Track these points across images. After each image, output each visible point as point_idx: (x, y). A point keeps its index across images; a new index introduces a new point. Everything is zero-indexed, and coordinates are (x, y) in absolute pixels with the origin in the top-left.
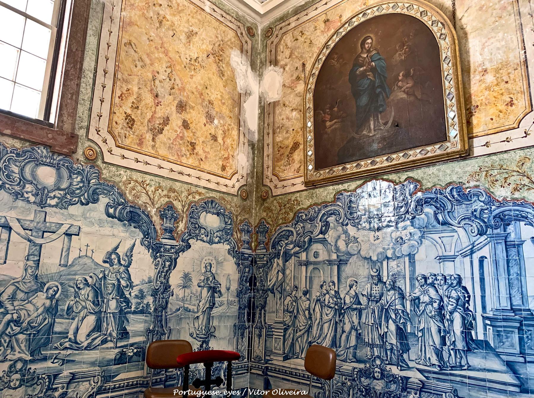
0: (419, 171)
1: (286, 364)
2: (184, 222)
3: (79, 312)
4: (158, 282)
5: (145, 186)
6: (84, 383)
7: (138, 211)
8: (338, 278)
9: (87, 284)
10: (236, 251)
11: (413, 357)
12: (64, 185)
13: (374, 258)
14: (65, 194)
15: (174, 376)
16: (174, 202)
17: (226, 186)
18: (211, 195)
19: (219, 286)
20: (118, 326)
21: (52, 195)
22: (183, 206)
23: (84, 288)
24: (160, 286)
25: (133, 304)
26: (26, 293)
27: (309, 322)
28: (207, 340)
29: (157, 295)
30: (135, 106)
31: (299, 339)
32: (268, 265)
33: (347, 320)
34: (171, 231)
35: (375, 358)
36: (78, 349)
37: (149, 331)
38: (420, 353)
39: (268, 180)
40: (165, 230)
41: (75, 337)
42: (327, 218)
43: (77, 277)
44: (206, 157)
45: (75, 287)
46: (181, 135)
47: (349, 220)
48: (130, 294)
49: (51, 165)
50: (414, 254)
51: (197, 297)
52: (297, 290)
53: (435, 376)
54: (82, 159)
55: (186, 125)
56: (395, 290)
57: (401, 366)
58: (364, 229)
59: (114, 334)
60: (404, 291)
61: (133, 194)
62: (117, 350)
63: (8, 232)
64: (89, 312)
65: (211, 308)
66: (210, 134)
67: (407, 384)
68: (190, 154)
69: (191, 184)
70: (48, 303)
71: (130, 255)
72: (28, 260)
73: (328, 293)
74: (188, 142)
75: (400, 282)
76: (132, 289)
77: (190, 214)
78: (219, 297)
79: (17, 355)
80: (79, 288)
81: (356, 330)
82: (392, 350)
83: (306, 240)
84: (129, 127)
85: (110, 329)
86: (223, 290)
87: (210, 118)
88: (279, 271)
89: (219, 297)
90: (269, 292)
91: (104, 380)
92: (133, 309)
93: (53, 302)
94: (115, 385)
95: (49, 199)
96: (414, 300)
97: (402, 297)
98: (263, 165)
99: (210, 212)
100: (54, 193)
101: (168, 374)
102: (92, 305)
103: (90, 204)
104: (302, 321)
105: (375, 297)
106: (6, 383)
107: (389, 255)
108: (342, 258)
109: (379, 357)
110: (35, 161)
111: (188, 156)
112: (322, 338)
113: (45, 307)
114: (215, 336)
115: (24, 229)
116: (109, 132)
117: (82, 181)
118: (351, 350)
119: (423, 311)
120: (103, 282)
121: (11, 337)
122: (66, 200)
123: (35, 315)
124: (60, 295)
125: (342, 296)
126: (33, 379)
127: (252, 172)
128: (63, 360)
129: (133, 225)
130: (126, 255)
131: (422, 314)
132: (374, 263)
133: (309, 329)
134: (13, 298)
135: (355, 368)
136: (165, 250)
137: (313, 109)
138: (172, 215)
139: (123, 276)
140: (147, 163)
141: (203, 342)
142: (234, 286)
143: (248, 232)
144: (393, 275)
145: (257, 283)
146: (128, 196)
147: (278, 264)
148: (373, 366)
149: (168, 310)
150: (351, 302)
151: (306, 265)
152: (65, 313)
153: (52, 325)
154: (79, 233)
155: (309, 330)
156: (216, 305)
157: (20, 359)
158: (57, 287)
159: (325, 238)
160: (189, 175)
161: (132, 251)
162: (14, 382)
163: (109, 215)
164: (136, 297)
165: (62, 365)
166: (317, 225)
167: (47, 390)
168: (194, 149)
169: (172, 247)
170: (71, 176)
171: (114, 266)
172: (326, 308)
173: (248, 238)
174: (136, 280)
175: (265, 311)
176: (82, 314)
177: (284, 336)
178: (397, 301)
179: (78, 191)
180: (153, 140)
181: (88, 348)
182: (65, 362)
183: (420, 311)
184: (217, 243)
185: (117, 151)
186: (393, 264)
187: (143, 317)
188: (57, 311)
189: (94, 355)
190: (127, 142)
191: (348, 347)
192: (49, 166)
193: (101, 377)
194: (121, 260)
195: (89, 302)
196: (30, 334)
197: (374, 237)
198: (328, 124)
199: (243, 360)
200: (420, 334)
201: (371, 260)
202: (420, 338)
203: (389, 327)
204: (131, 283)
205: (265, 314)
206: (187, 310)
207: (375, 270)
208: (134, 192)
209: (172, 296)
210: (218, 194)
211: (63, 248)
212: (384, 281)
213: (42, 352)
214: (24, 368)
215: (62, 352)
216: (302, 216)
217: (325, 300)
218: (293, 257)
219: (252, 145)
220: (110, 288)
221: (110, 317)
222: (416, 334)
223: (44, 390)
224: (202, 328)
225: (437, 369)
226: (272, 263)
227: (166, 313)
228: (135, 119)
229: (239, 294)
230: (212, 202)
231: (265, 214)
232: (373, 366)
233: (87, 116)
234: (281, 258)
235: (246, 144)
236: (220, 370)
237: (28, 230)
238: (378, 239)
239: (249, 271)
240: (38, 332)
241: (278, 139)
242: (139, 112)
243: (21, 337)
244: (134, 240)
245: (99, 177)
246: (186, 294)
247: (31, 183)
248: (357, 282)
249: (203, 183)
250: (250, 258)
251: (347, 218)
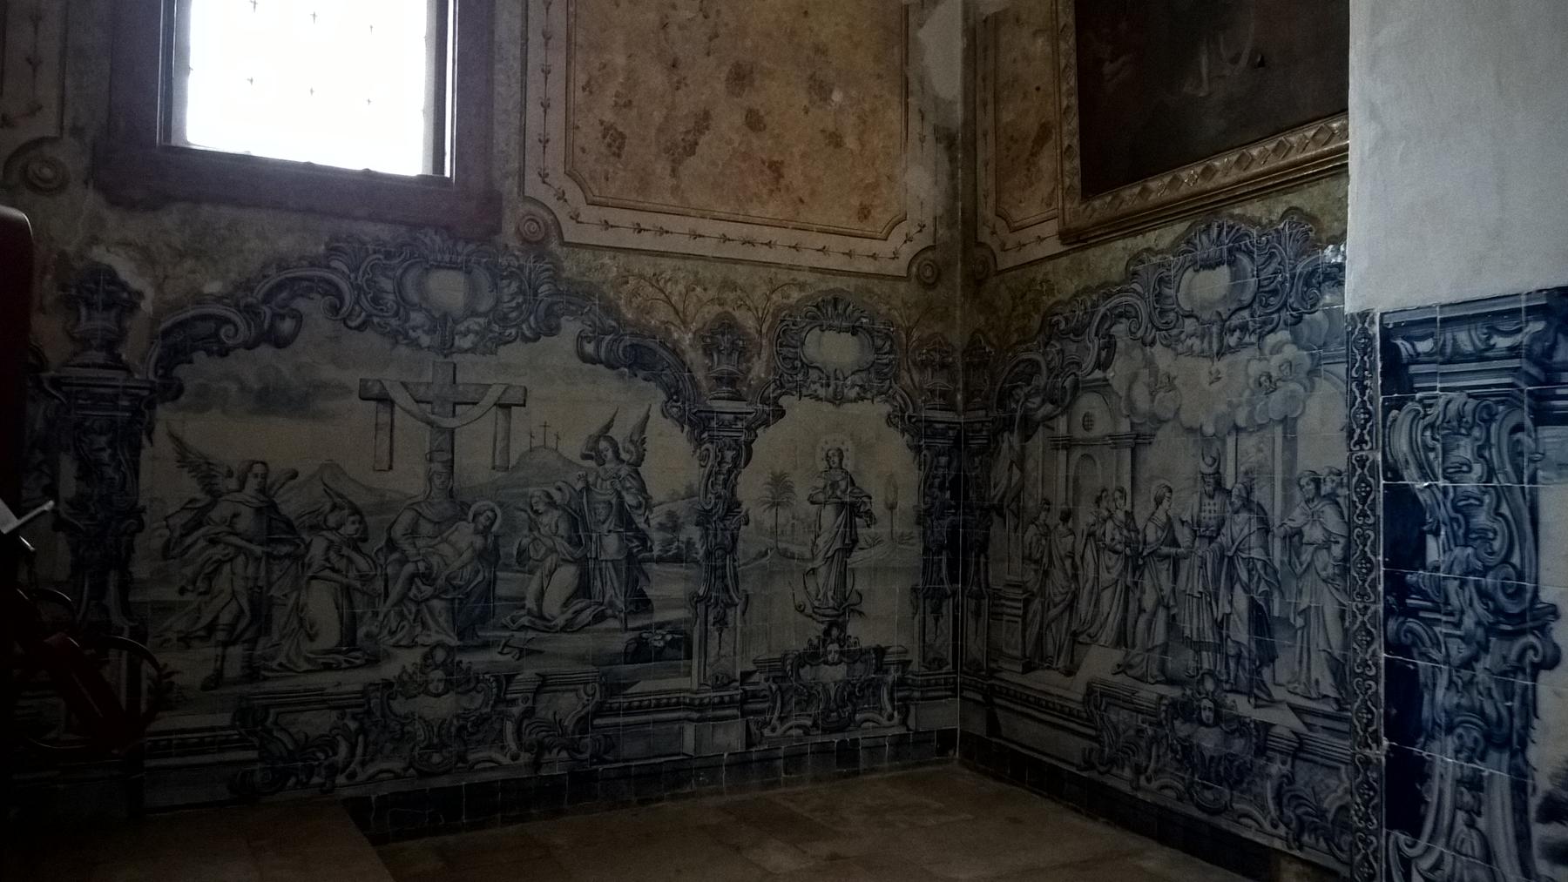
0: (1315, 190)
1: (1031, 680)
2: (764, 355)
3: (541, 560)
4: (709, 495)
5: (662, 283)
6: (566, 695)
7: (650, 343)
8: (1133, 479)
9: (552, 503)
10: (910, 417)
11: (1283, 676)
12: (484, 307)
13: (1209, 430)
14: (489, 323)
15: (764, 693)
16: (737, 314)
17: (874, 256)
18: (832, 286)
19: (865, 499)
20: (627, 587)
21: (463, 329)
22: (761, 321)
23: (546, 512)
24: (716, 504)
25: (656, 543)
26: (435, 523)
27: (1073, 586)
28: (840, 620)
29: (709, 522)
30: (621, 102)
31: (1053, 625)
32: (990, 450)
33: (1147, 582)
34: (732, 380)
35: (1203, 675)
36: (548, 629)
37: (695, 600)
38: (1297, 668)
39: (987, 231)
40: (719, 379)
41: (540, 607)
42: (1111, 327)
43: (531, 490)
44: (813, 193)
45: (529, 511)
46: (743, 149)
47: (1159, 329)
48: (647, 521)
49: (453, 266)
50: (1295, 419)
51: (810, 527)
52: (1049, 510)
53: (1328, 723)
54: (514, 243)
55: (754, 121)
56: (1250, 510)
57: (1257, 697)
58: (1190, 352)
59: (620, 604)
60: (1270, 513)
61: (634, 305)
62: (628, 636)
63: (389, 409)
64: (563, 560)
65: (848, 550)
66: (823, 131)
67: (1266, 740)
68: (772, 191)
69: (778, 265)
70: (479, 542)
71: (639, 439)
72: (431, 460)
73: (1111, 516)
74: (763, 162)
75: (1260, 489)
76: (651, 512)
77: (779, 337)
78: (869, 526)
79: (435, 638)
80: (536, 512)
81: (1168, 608)
82: (1239, 656)
83: (1067, 384)
84: (614, 154)
85: (609, 592)
86: (878, 508)
87: (820, 90)
88: (1012, 462)
89: (869, 526)
90: (994, 514)
91: (607, 690)
92: (656, 552)
93: (489, 540)
94: (630, 703)
95: (457, 337)
96: (1291, 537)
97: (1265, 529)
98: (976, 190)
99: (830, 327)
100: (466, 324)
101: (747, 688)
102: (566, 544)
103: (543, 338)
104: (1058, 583)
105: (1207, 527)
106: (420, 685)
107: (1241, 422)
108: (1142, 430)
109: (1211, 673)
110: (420, 262)
111: (765, 197)
112: (1098, 623)
113: (474, 551)
114: (861, 613)
115: (417, 402)
116: (569, 174)
117: (521, 291)
118: (1156, 655)
119: (1309, 565)
120: (585, 500)
121: (418, 603)
122: (491, 335)
123: (457, 564)
124: (501, 527)
125: (1140, 525)
126: (468, 681)
127: (951, 211)
128: (521, 650)
129: (641, 374)
130: (631, 441)
131: (1305, 571)
132: (1207, 441)
133: (1072, 601)
134: (413, 532)
135: (1162, 697)
136: (722, 425)
137: (1074, 29)
138: (733, 343)
139: (628, 485)
140: (663, 232)
141: (831, 625)
142: (908, 501)
143: (943, 366)
144: (1246, 473)
145: (971, 493)
146: (624, 310)
147: (1011, 447)
148: (1200, 694)
149: (739, 554)
150: (1158, 540)
151: (1067, 449)
152: (513, 561)
153: (492, 583)
154: (525, 401)
155: (1071, 606)
156: (862, 543)
157: (440, 645)
158: (493, 510)
159: (1106, 380)
160: (769, 244)
161: (643, 431)
162: (435, 683)
163: (585, 358)
164: (662, 527)
165: (518, 659)
166: (1090, 345)
167: (496, 703)
168: (781, 176)
169: (738, 416)
170: (496, 285)
171: (607, 466)
172: (1106, 552)
173: (944, 382)
174: (656, 491)
175: (987, 557)
176: (549, 562)
177: (1024, 616)
178: (1253, 538)
179: (514, 315)
180: (674, 172)
181: (568, 627)
182: (525, 652)
183: (1301, 565)
184: (855, 401)
186: (1248, 443)
187: (682, 570)
188: (498, 557)
189: (581, 643)
191: (1150, 646)
192: (449, 268)
193: (601, 686)
194: (621, 451)
195: (559, 540)
196: (453, 600)
197: (1210, 373)
198: (1108, 68)
199: (941, 668)
200: (1300, 622)
201: (1202, 434)
202: (1299, 633)
203: (1235, 604)
204: (648, 499)
205: (986, 564)
206: (785, 555)
207: (1209, 460)
208: (637, 301)
209: (747, 523)
210: (853, 281)
211: (496, 433)
212: (1229, 487)
213: (479, 634)
214: (450, 660)
215: (517, 634)
216: (1058, 323)
217: (1104, 534)
218: (1041, 428)
219: (947, 139)
220: (602, 512)
221: (606, 568)
222: (1292, 621)
223: (491, 702)
224: (825, 595)
225: (1330, 708)
226: (998, 442)
227: (734, 560)
228: (627, 132)
229: (923, 518)
230: (836, 301)
231: (982, 319)
232: (1200, 694)
233: (517, 148)
234: (1016, 431)
235: (930, 138)
236: (878, 687)
237: (423, 402)
238: (1219, 379)
239: (949, 463)
240: (468, 595)
241: (1007, 117)
242: (634, 112)
243: (436, 603)
244: (647, 407)
245: (555, 279)
246: (781, 520)
247: (420, 309)
248: (1170, 491)
249: (808, 258)
250: (951, 433)
251: (1153, 325)
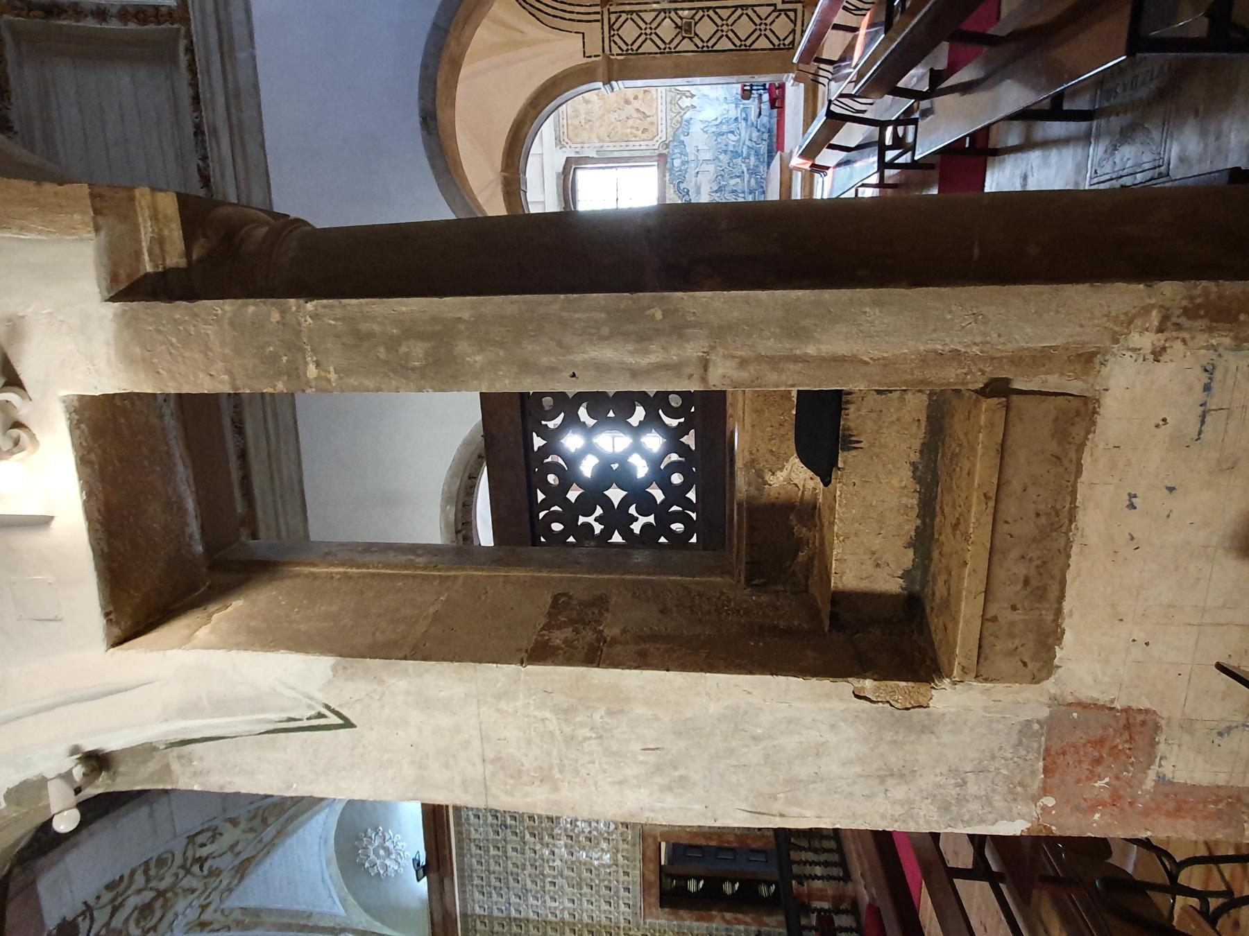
12: (679, 155)
181: (740, 135)
182: (744, 144)
185: (660, 135)
190: (655, 130)
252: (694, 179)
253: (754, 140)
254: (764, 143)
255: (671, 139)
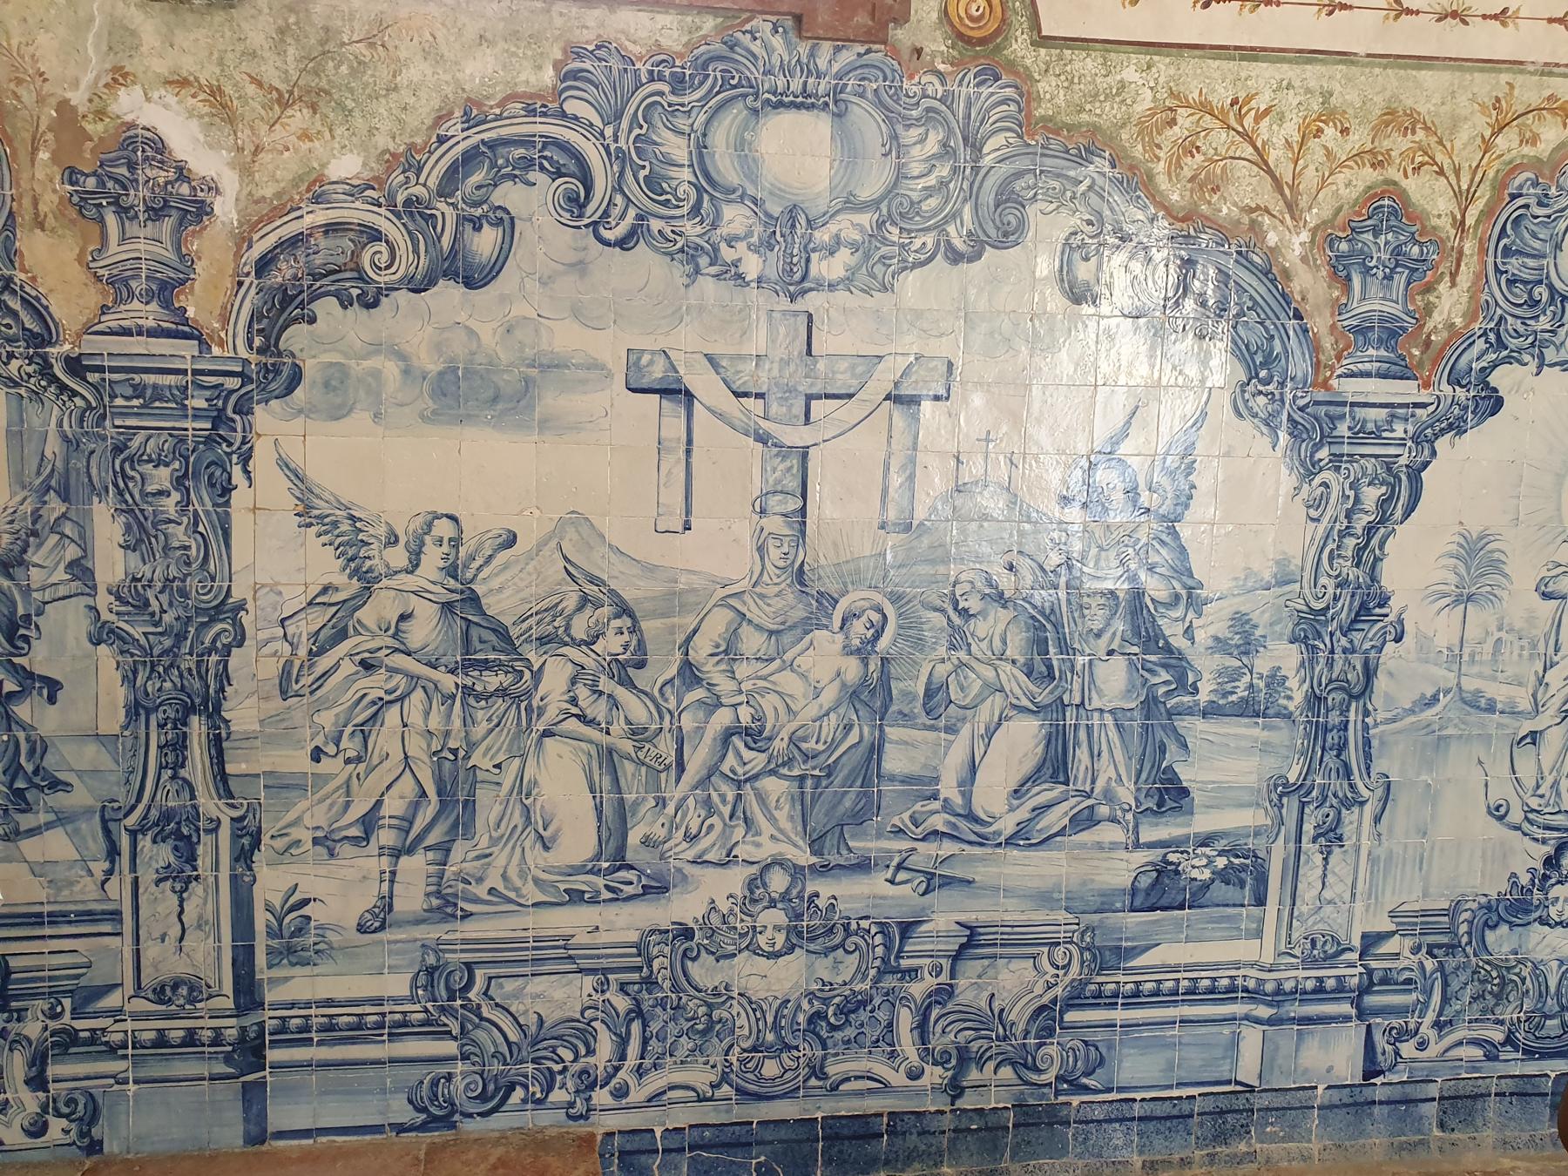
12: (872, 185)
181: (1020, 838)
182: (934, 882)
252: (609, 347)
253: (970, 988)
254: (934, 1075)
255: (1052, 94)
